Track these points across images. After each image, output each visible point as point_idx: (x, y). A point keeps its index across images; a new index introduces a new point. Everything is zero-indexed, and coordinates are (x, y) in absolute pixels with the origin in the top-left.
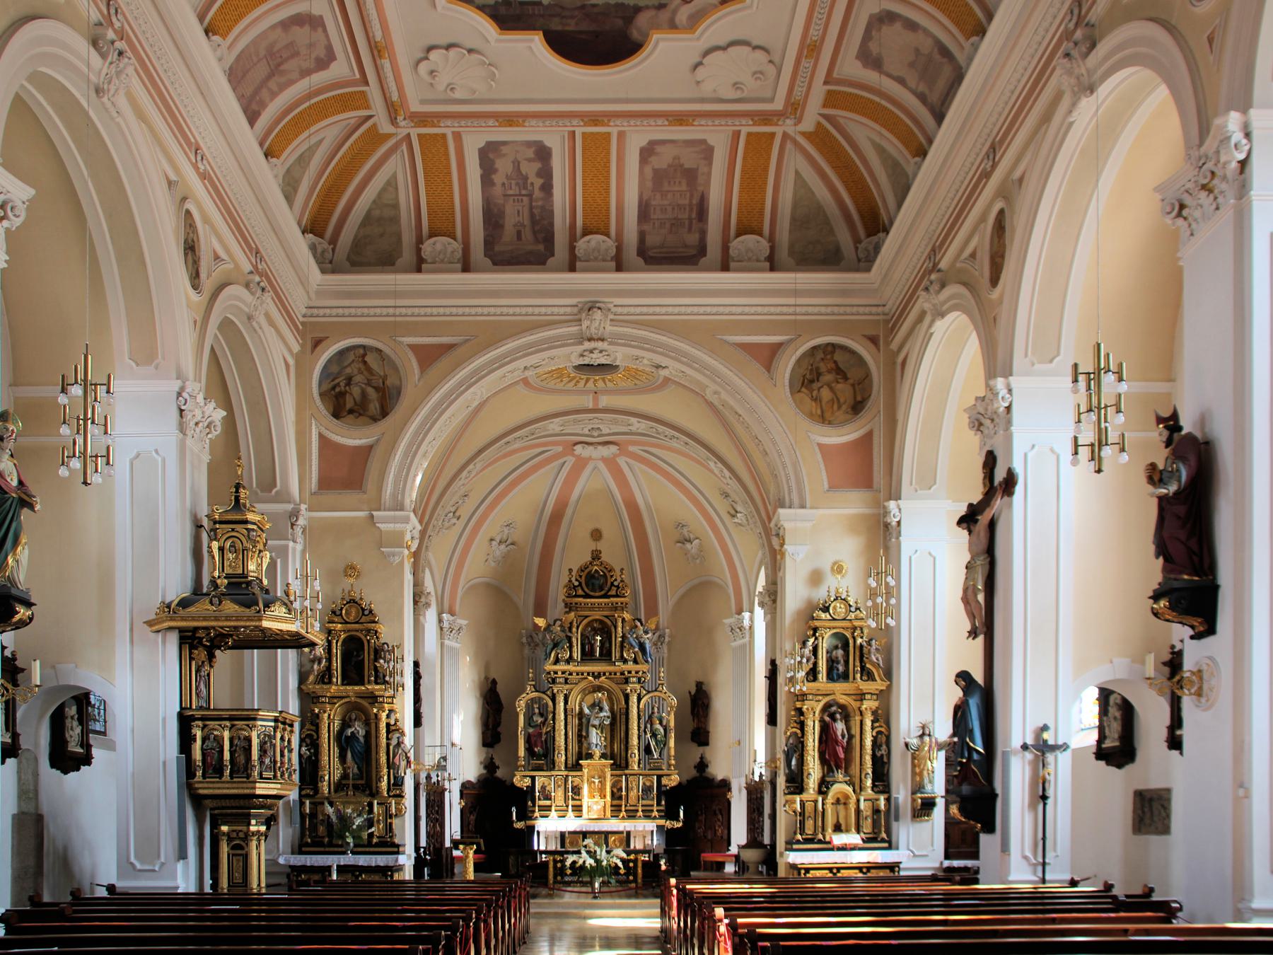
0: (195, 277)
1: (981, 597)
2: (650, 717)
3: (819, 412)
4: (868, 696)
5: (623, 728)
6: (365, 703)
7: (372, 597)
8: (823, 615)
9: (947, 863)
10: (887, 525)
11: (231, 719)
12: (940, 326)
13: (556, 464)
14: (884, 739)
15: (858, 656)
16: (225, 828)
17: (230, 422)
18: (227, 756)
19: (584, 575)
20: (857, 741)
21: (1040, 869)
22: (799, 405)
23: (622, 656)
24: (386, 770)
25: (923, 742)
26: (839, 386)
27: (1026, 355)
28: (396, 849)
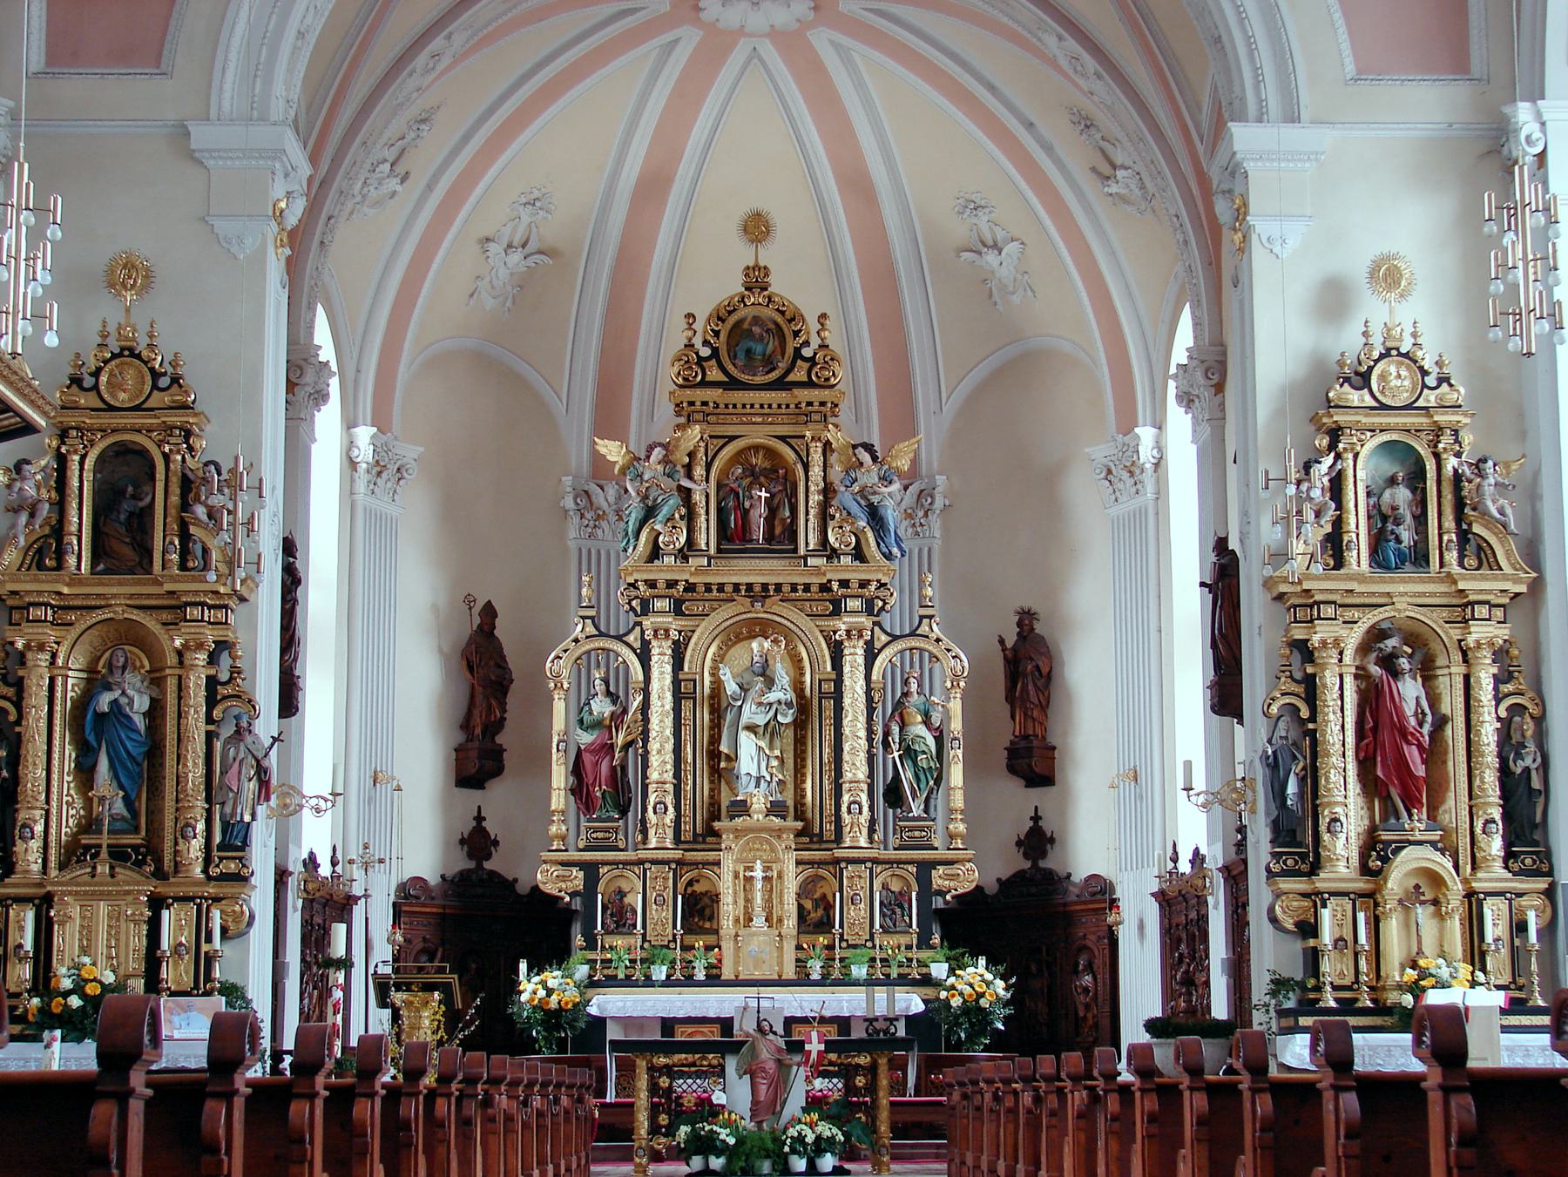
2: (899, 706)
5: (829, 732)
6: (150, 622)
7: (175, 335)
8: (1355, 397)
14: (1529, 727)
20: (1455, 733)
23: (824, 541)
24: (201, 804)
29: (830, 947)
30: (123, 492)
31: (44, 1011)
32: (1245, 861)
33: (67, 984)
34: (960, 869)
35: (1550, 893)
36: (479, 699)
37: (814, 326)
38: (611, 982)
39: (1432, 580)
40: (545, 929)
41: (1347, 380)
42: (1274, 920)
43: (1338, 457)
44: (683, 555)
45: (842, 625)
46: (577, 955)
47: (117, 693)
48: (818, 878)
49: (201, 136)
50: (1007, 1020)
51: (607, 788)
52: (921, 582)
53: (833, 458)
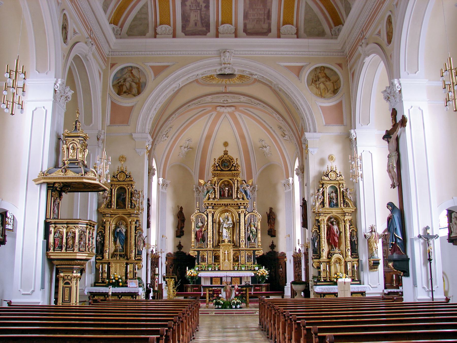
0: (65, 39)
1: (395, 170)
2: (250, 224)
3: (320, 93)
4: (347, 214)
6: (126, 217)
7: (130, 169)
8: (326, 178)
9: (386, 291)
10: (351, 140)
11: (67, 223)
12: (367, 60)
13: (209, 115)
14: (355, 233)
15: (341, 196)
16: (62, 274)
17: (75, 96)
18: (64, 240)
19: (220, 161)
21: (431, 293)
24: (134, 247)
27: (405, 70)
29: (238, 264)
31: (109, 282)
32: (308, 253)
33: (113, 278)
35: (358, 261)
36: (180, 223)
37: (235, 160)
38: (202, 270)
42: (313, 266)
43: (323, 188)
44: (214, 199)
45: (240, 211)
46: (196, 266)
48: (236, 253)
49: (134, 136)
50: (268, 278)
51: (201, 238)
52: (253, 203)
53: (239, 182)
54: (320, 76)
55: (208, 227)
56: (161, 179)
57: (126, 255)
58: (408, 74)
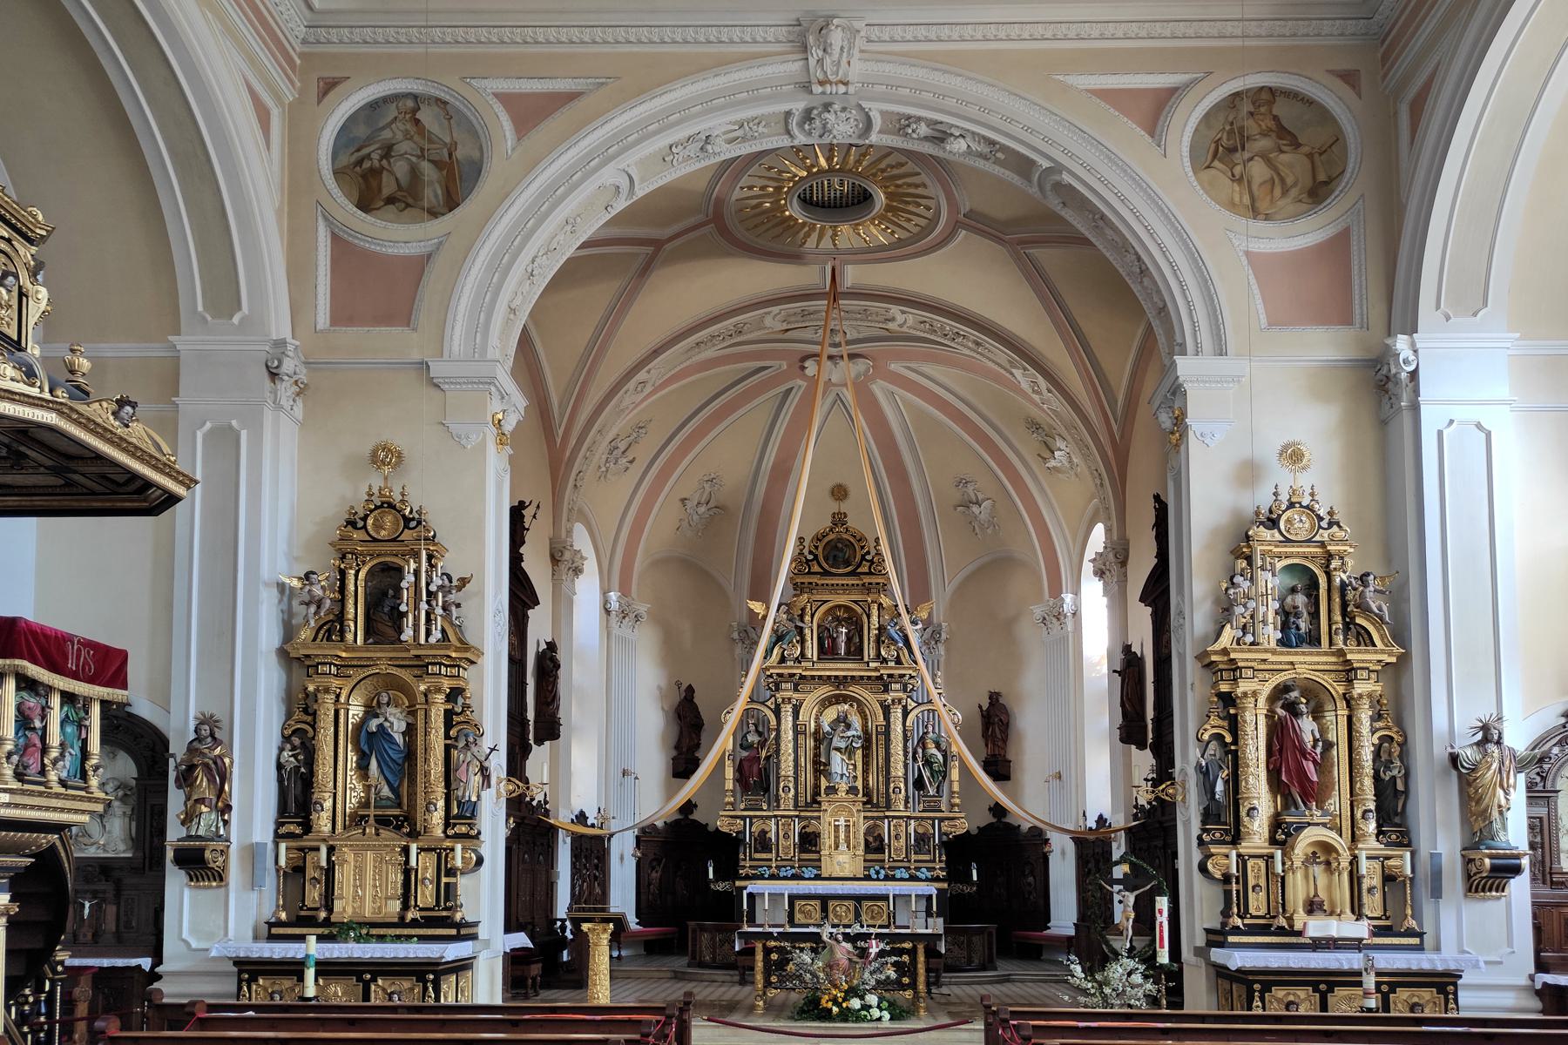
3: (1247, 200)
5: (882, 752)
6: (405, 675)
14: (1396, 750)
22: (1209, 188)
23: (879, 655)
25: (1485, 754)
26: (1284, 157)
27: (1438, 307)
28: (464, 931)
30: (385, 594)
34: (957, 822)
39: (1326, 654)
40: (726, 849)
41: (1262, 523)
45: (889, 697)
47: (381, 720)
48: (875, 826)
49: (437, 370)
51: (756, 776)
54: (1251, 126)
55: (778, 745)
56: (613, 596)
57: (409, 818)
58: (1448, 318)
